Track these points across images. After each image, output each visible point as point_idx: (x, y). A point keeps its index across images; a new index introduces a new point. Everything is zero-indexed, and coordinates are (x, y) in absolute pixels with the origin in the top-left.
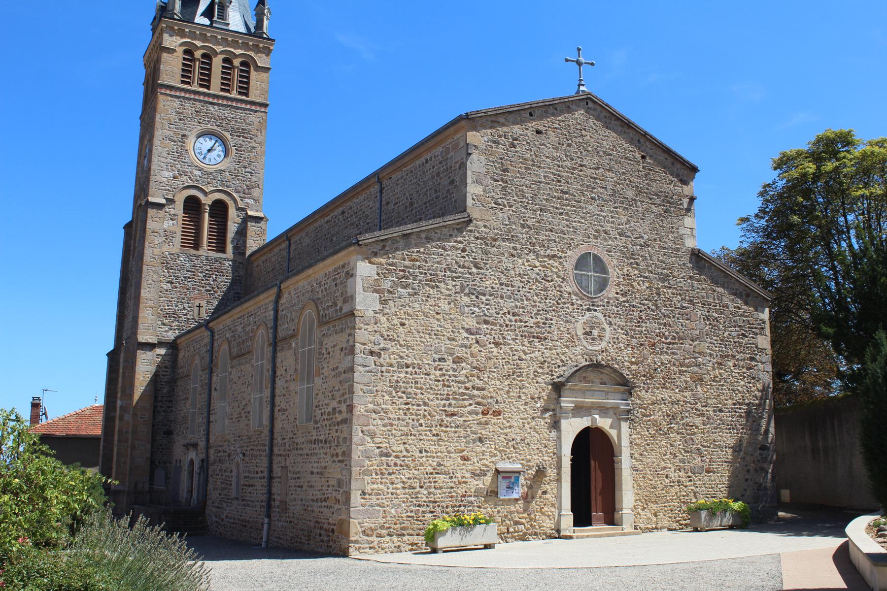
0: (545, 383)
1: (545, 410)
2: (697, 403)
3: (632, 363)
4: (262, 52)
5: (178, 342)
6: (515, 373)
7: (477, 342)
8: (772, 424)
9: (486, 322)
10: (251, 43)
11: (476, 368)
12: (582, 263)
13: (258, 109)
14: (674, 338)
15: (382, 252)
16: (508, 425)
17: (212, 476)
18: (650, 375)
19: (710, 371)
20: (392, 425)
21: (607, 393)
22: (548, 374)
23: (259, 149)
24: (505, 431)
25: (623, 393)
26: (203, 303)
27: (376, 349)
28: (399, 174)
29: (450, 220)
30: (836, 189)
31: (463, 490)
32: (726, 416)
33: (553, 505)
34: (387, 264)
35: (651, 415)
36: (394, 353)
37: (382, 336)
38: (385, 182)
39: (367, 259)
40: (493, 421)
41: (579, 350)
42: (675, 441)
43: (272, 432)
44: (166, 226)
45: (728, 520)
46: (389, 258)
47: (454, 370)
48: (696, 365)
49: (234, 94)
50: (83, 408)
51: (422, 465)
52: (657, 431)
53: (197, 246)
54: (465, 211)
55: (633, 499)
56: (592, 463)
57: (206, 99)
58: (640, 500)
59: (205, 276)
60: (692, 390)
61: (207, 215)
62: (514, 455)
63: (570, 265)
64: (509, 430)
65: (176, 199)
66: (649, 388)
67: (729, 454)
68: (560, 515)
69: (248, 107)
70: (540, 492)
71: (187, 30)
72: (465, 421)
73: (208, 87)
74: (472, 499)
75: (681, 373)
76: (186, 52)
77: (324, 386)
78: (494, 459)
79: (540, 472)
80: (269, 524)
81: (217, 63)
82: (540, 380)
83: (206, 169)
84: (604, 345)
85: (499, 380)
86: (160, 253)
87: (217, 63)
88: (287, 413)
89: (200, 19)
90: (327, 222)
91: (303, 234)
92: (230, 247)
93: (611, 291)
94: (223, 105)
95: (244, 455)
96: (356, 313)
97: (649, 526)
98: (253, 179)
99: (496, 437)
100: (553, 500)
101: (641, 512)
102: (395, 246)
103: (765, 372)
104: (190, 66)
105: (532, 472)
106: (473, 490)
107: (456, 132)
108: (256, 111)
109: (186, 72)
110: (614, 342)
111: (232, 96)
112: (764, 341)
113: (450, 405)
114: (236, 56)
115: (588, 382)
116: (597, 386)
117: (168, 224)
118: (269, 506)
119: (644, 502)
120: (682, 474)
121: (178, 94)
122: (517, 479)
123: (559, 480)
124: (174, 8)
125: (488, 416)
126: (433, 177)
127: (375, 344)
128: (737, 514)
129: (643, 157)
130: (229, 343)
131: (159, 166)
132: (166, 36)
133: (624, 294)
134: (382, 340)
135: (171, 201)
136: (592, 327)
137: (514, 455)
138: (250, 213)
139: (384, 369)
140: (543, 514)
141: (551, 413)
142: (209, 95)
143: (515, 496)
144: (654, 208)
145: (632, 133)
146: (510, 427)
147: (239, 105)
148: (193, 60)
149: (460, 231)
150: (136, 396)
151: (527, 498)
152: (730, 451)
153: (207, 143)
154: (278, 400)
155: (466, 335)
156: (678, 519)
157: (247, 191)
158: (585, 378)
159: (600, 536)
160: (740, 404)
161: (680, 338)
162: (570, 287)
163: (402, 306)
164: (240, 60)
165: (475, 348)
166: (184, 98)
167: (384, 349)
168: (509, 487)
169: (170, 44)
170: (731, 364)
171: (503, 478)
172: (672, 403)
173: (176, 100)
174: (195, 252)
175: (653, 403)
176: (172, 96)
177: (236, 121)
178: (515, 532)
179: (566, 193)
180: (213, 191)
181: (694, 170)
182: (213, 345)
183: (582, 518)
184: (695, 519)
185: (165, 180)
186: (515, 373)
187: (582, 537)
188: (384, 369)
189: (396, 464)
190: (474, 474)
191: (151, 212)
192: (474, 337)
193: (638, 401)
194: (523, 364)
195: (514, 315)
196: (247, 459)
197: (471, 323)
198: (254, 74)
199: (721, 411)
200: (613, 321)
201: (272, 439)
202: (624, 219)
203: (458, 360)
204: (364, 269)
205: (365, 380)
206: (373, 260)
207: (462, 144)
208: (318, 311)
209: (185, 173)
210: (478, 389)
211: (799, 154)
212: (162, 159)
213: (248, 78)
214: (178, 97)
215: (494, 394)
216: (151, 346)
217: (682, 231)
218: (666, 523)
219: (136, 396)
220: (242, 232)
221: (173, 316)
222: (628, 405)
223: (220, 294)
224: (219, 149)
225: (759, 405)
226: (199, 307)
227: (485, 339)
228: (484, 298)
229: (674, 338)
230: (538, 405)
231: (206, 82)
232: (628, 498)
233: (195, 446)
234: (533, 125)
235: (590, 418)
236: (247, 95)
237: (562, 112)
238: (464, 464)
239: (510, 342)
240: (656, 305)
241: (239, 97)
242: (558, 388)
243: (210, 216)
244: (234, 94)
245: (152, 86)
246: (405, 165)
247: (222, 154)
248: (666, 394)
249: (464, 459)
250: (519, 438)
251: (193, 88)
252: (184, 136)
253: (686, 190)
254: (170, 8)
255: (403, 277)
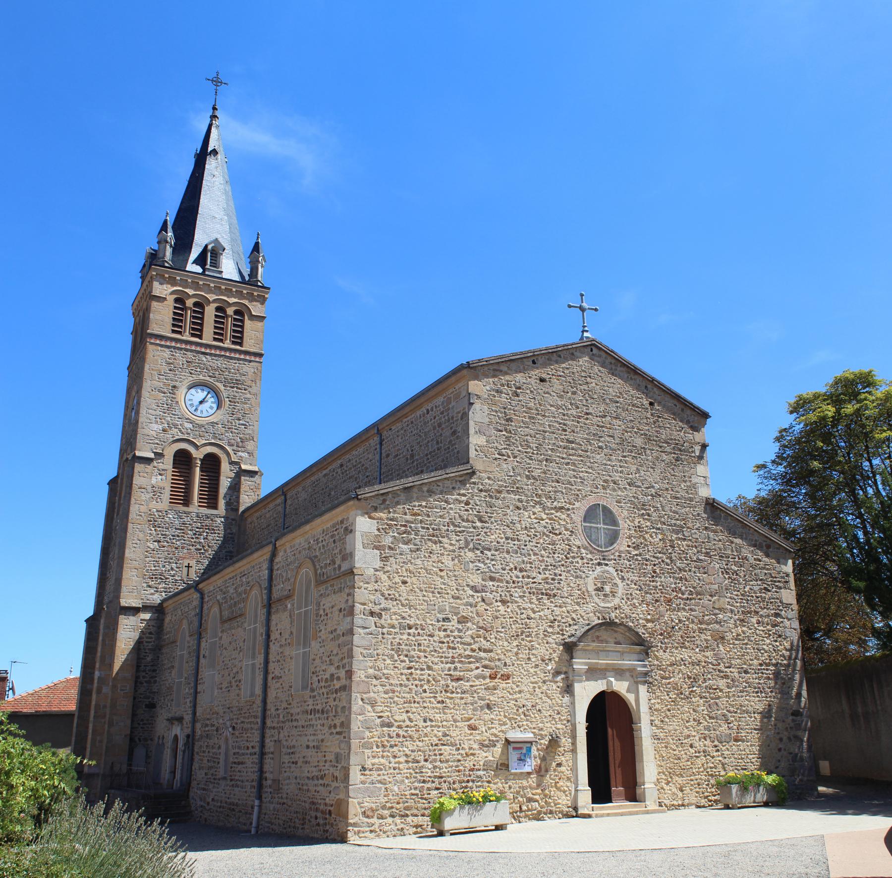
0: (556, 643)
1: (557, 673)
2: (719, 664)
3: (648, 621)
4: (257, 301)
5: (165, 605)
6: (523, 633)
7: (483, 600)
8: (805, 687)
9: (492, 579)
10: (245, 292)
11: (482, 628)
12: (590, 514)
13: (253, 358)
14: (691, 593)
15: (382, 506)
16: (517, 689)
17: (198, 753)
18: (668, 634)
19: (732, 629)
20: (393, 692)
21: (622, 653)
22: (558, 633)
23: (253, 401)
24: (515, 696)
25: (640, 653)
26: (193, 563)
27: (376, 609)
28: (399, 425)
29: (453, 472)
30: (858, 432)
31: (471, 763)
32: (752, 677)
33: (569, 779)
34: (387, 519)
35: (670, 678)
36: (395, 614)
37: (383, 595)
38: (385, 434)
39: (367, 513)
40: (501, 686)
41: (590, 607)
42: (698, 706)
43: (264, 701)
44: (154, 481)
45: (762, 796)
46: (390, 512)
47: (459, 631)
48: (716, 622)
49: (227, 344)
50: (56, 681)
51: (426, 735)
52: (678, 695)
53: (187, 502)
54: (468, 462)
55: (656, 772)
56: (610, 730)
57: (198, 349)
58: (663, 773)
59: (195, 534)
60: (714, 650)
61: (198, 469)
62: (525, 723)
63: (578, 517)
64: (519, 695)
65: (165, 453)
66: (667, 648)
67: (755, 721)
68: (576, 791)
69: (242, 357)
70: (554, 764)
71: (178, 278)
72: (472, 686)
73: (200, 337)
74: (481, 773)
75: (701, 631)
76: (177, 300)
77: (322, 650)
78: (503, 728)
79: (554, 742)
80: (260, 806)
81: (210, 312)
82: (550, 640)
83: (197, 422)
84: (617, 601)
85: (507, 640)
86: (147, 511)
87: (210, 312)
88: (281, 680)
89: (192, 267)
90: (325, 475)
91: (300, 489)
92: (222, 503)
93: (622, 545)
94: (215, 355)
95: (234, 728)
96: (355, 571)
97: (675, 803)
98: (247, 431)
99: (505, 703)
100: (568, 773)
101: (665, 786)
102: (396, 500)
103: (792, 628)
104: (182, 315)
105: (545, 742)
106: (481, 763)
107: (457, 381)
108: (250, 361)
109: (177, 322)
110: (628, 599)
111: (226, 345)
112: (789, 596)
113: (455, 668)
114: (230, 305)
115: (602, 642)
116: (611, 646)
117: (156, 480)
118: (260, 786)
119: (668, 774)
120: (708, 742)
121: (168, 344)
122: (529, 750)
123: (574, 751)
124: (165, 255)
125: (496, 680)
126: (434, 428)
127: (375, 604)
128: (771, 789)
129: (651, 404)
130: (220, 605)
131: (147, 418)
132: (156, 284)
133: (637, 547)
134: (383, 600)
135: (159, 455)
136: (603, 583)
137: (525, 723)
138: (244, 467)
139: (385, 630)
140: (558, 789)
141: (563, 676)
142: (240, 352)
143: (527, 769)
144: (665, 457)
145: (639, 380)
146: (520, 692)
147: (233, 355)
148: (184, 309)
149: (463, 483)
150: (117, 667)
151: (541, 772)
152: (758, 716)
153: (198, 394)
154: (271, 666)
155: (471, 593)
156: (706, 794)
157: (240, 444)
158: (598, 637)
159: (622, 814)
160: (767, 665)
161: (698, 593)
162: (579, 540)
163: (404, 562)
164: (234, 308)
165: (481, 607)
166: (175, 348)
167: (385, 609)
168: (520, 760)
169: (160, 293)
170: (754, 620)
171: (514, 748)
172: (693, 664)
173: (167, 350)
174: (185, 509)
175: (672, 665)
176: (162, 346)
177: (229, 372)
178: (529, 810)
179: (572, 442)
180: (205, 445)
181: (705, 416)
182: (202, 607)
183: (601, 795)
184: (726, 795)
185: (154, 433)
186: (523, 633)
187: (602, 816)
188: (385, 630)
189: (398, 735)
190: (482, 745)
191: (138, 467)
192: (479, 594)
193: (656, 662)
194: (532, 623)
195: (521, 570)
196: (237, 733)
197: (476, 579)
198: (248, 323)
199: (746, 672)
200: (626, 576)
201: (265, 710)
202: (633, 468)
203: (463, 620)
204: (364, 525)
205: (365, 643)
206: (373, 515)
207: (464, 393)
208: (316, 570)
209: (176, 426)
210: (485, 651)
211: (816, 396)
212: (150, 411)
213: (242, 327)
214: (168, 347)
215: (502, 657)
216: (135, 611)
217: (694, 480)
218: (693, 800)
219: (117, 667)
220: (235, 487)
221: (161, 577)
222: (645, 666)
223: (210, 553)
224: (211, 401)
225: (788, 665)
226: (188, 567)
227: (492, 596)
228: (489, 553)
229: (691, 593)
230: (549, 668)
231: (198, 331)
232: (650, 770)
233: (180, 720)
234: (536, 373)
235: (605, 681)
236: (241, 344)
237: (566, 359)
238: (471, 734)
239: (518, 600)
240: (671, 558)
241: (233, 347)
242: (570, 648)
243: (201, 471)
244: (227, 344)
245: (141, 336)
246: (405, 416)
247: (215, 406)
248: (685, 654)
249: (472, 728)
250: (530, 704)
251: (184, 338)
252: (174, 387)
253: (698, 437)
254: (161, 255)
255: (404, 533)
